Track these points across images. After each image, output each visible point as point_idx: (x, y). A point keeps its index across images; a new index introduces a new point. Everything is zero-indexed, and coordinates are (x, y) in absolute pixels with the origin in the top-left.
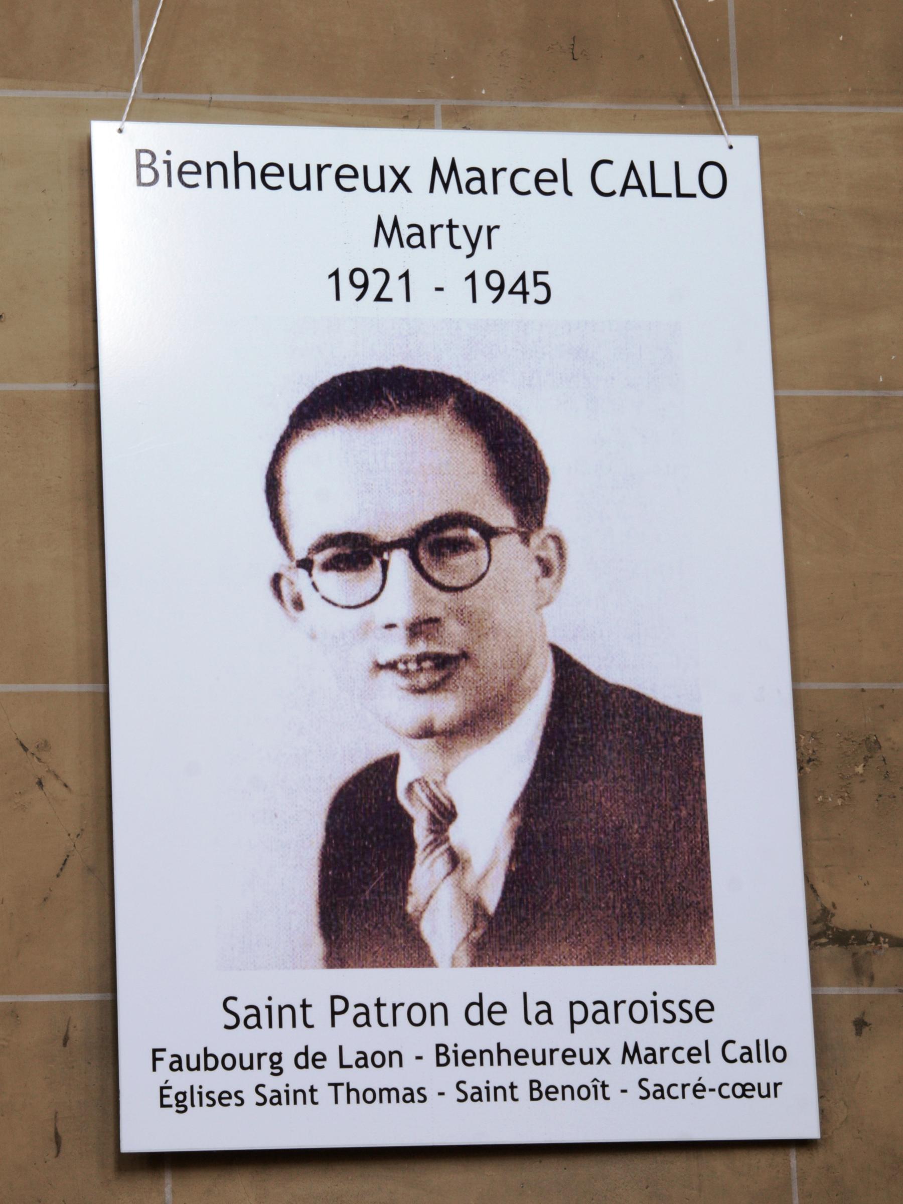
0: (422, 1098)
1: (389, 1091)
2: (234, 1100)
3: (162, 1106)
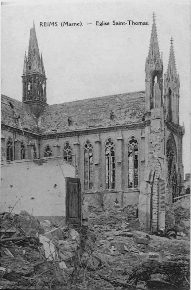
0: (56, 25)
1: (97, 23)
2: (115, 22)
3: (97, 25)
